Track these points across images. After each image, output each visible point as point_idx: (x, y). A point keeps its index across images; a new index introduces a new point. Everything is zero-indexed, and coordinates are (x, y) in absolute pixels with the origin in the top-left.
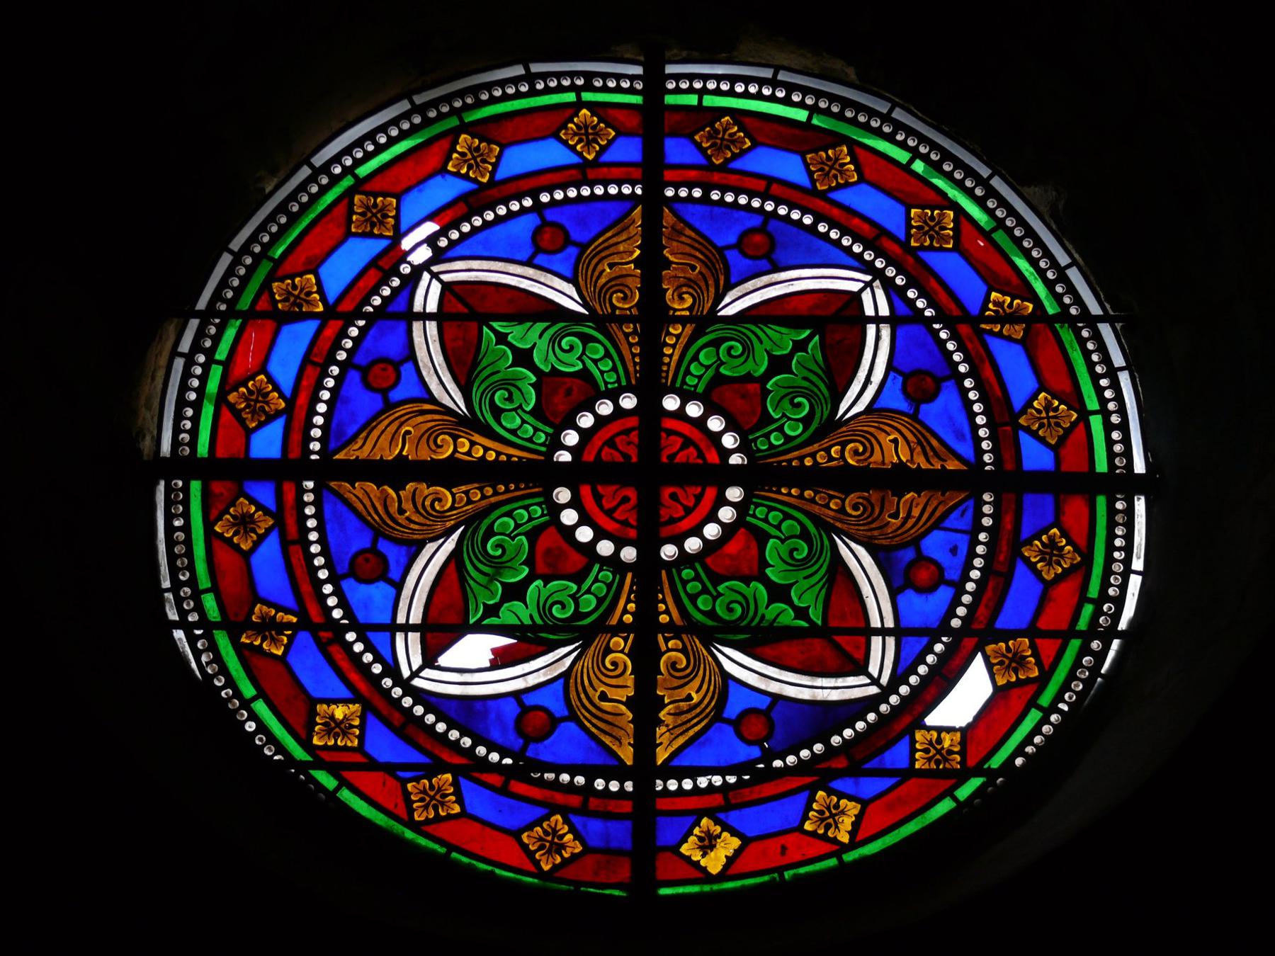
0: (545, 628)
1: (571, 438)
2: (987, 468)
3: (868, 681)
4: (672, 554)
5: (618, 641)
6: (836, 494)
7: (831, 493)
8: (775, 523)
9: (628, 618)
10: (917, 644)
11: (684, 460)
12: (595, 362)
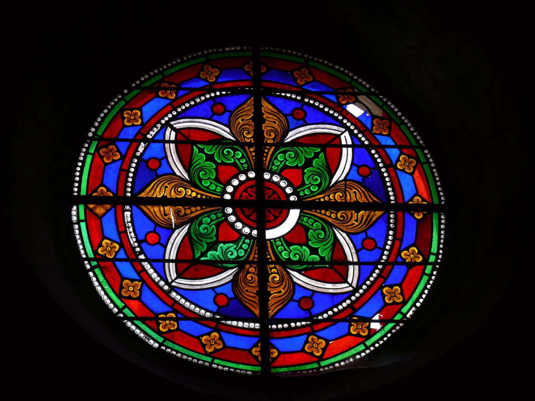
1: (230, 189)
2: (392, 202)
3: (348, 285)
4: (250, 174)
6: (333, 211)
7: (331, 211)
8: (218, 187)
11: (273, 199)
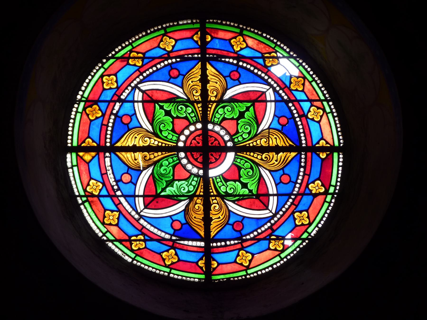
0: (177, 196)
1: (183, 138)
5: (199, 201)
9: (202, 194)
10: (130, 98)
12: (189, 114)
